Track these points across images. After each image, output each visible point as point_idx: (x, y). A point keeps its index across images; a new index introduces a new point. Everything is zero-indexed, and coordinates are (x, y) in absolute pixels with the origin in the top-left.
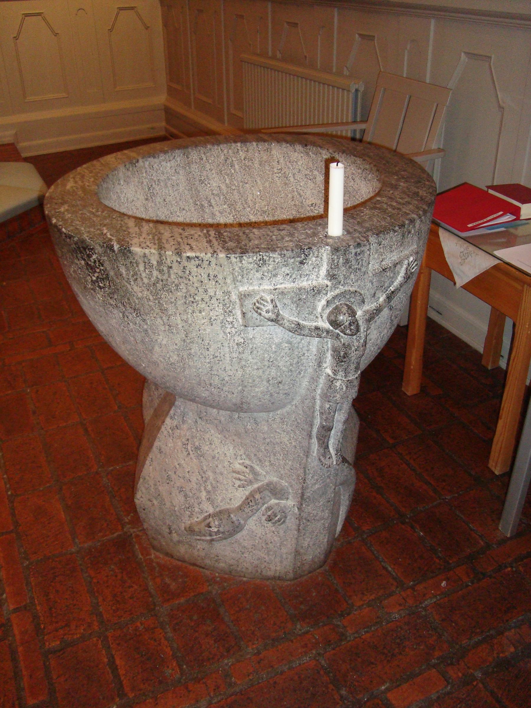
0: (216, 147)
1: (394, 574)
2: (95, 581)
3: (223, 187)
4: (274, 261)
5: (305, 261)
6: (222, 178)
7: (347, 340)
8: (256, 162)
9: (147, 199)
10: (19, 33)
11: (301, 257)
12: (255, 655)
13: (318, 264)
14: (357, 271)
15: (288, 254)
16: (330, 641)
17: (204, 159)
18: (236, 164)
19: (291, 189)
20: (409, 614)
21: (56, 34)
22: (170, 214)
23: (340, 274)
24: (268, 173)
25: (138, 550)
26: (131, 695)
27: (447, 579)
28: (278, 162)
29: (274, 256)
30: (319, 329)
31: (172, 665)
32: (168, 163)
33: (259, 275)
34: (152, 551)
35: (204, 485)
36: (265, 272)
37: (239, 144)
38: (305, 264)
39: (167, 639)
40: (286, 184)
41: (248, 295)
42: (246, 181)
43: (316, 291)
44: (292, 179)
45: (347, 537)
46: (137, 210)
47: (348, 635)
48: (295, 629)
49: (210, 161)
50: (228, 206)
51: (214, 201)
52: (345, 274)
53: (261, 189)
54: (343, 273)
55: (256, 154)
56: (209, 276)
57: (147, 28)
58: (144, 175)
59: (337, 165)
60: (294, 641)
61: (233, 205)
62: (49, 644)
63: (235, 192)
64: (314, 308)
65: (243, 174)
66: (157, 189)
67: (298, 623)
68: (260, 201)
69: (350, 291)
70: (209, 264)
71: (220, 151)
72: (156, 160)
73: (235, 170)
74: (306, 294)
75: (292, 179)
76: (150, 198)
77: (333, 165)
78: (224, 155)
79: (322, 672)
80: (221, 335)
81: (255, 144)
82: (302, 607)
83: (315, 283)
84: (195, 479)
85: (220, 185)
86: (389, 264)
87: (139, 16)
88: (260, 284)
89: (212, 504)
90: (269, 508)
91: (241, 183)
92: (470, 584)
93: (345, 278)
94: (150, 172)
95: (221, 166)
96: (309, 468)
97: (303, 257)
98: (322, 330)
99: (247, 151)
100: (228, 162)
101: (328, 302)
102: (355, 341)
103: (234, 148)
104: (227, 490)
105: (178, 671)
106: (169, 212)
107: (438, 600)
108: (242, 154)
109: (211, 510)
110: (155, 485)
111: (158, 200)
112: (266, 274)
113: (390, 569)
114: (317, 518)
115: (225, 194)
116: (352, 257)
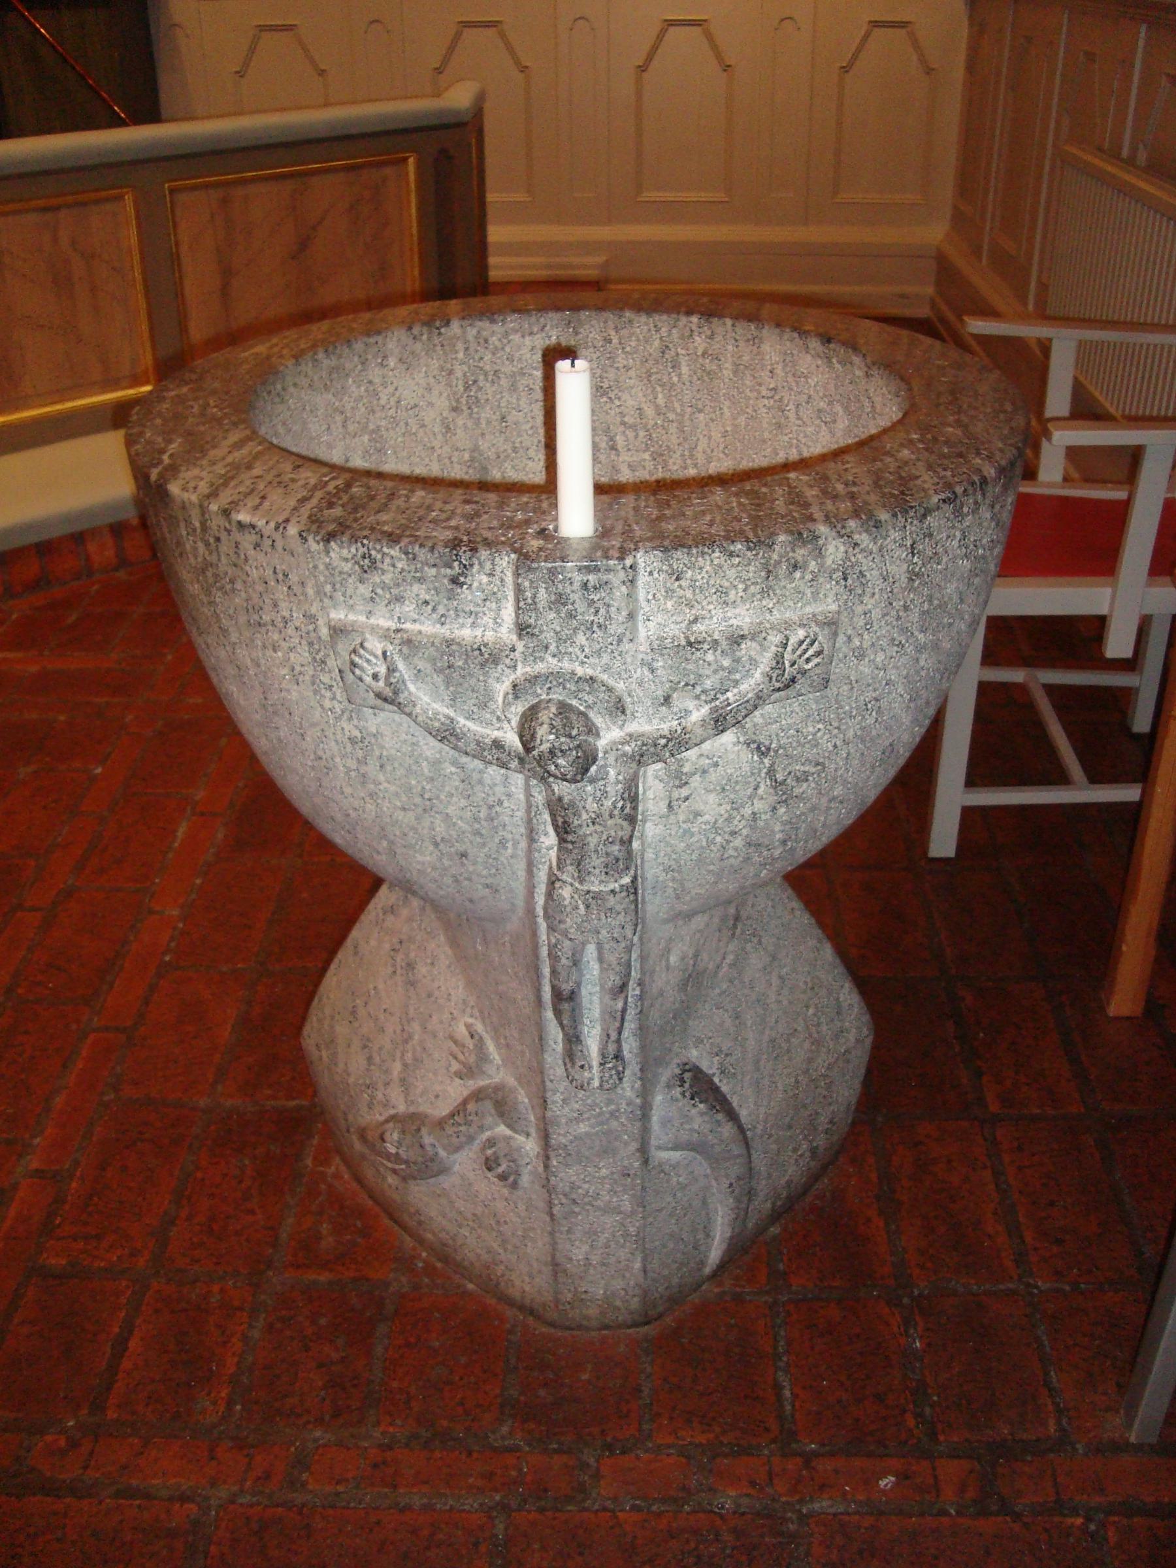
0: (643, 318)
1: (788, 1408)
2: (199, 1175)
3: (650, 412)
4: (394, 566)
5: (462, 579)
6: (649, 391)
7: (569, 791)
8: (727, 365)
9: (455, 409)
10: (650, 58)
11: (451, 567)
12: (380, 1446)
13: (494, 593)
14: (595, 628)
15: (422, 554)
16: (546, 1490)
17: (615, 341)
18: (684, 364)
19: (786, 438)
20: (758, 1514)
21: (727, 68)
22: (510, 451)
23: (545, 628)
24: (749, 394)
25: (313, 1149)
26: (112, 1414)
27: (903, 1476)
28: (771, 372)
29: (392, 552)
30: (502, 747)
31: (219, 1392)
32: (527, 338)
33: (364, 590)
34: (337, 1160)
35: (402, 1048)
36: (378, 586)
37: (695, 319)
38: (465, 587)
39: (245, 1338)
40: (779, 426)
41: (341, 631)
42: (700, 406)
43: (487, 656)
44: (792, 415)
45: (743, 1283)
46: (421, 427)
47: (594, 1495)
48: (493, 1432)
49: (628, 349)
50: (651, 455)
51: (624, 438)
52: (558, 629)
53: (729, 429)
54: (553, 626)
55: (730, 347)
56: (275, 572)
57: (929, 71)
58: (461, 355)
59: (573, 365)
60: (475, 1455)
61: (662, 455)
62: (48, 1258)
63: (673, 428)
64: (489, 697)
65: (696, 388)
66: (488, 392)
67: (510, 1422)
68: (721, 455)
69: (573, 673)
70: (273, 545)
71: (653, 329)
72: (498, 328)
73: (679, 376)
74: (464, 657)
75: (792, 415)
76: (465, 408)
77: (563, 365)
78: (661, 338)
79: (483, 1548)
80: (318, 713)
81: (729, 322)
82: (542, 1392)
83: (490, 636)
84: (391, 1030)
85: (643, 405)
86: (717, 633)
87: (916, 44)
88: (370, 612)
89: (406, 1092)
90: (491, 1143)
91: (690, 409)
92: (953, 1512)
93: (560, 640)
94: (477, 351)
95: (651, 362)
96: (552, 1077)
97: (457, 568)
98: (509, 753)
99: (711, 337)
100: (667, 356)
101: (515, 686)
102: (590, 799)
103: (685, 326)
104: (435, 1074)
105: (222, 1409)
106: (508, 447)
107: (848, 1514)
108: (700, 343)
109: (402, 1108)
110: (333, 1018)
111: (486, 413)
112: (379, 591)
113: (787, 1393)
114: (599, 1203)
115: (649, 427)
116: (573, 592)
